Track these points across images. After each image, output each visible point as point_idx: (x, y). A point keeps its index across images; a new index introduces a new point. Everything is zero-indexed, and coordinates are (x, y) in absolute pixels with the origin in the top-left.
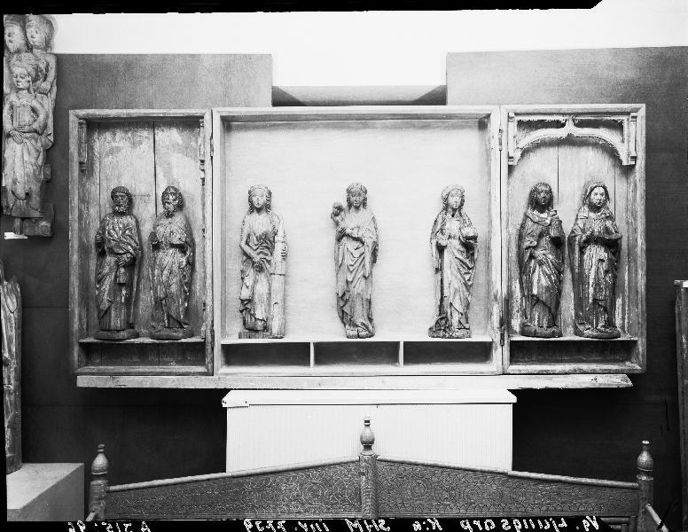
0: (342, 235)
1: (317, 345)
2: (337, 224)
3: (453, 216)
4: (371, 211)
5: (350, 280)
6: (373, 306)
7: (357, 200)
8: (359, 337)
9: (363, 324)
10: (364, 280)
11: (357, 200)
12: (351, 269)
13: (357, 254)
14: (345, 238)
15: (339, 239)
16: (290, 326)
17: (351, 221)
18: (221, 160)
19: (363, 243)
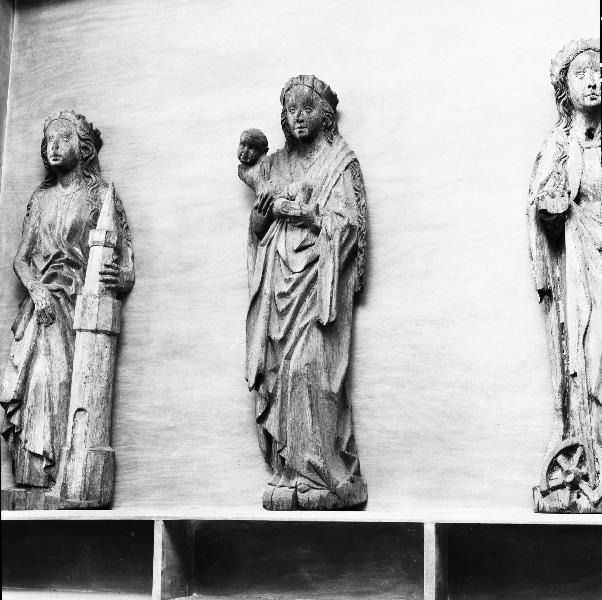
0: (266, 219)
1: (449, 534)
2: (252, 185)
3: (594, 186)
4: (346, 145)
5: (277, 336)
6: (129, 351)
7: (314, 120)
8: (296, 506)
9: (312, 467)
10: (317, 338)
11: (314, 120)
12: (282, 305)
13: (299, 262)
14: (274, 226)
15: (258, 232)
16: (125, 481)
17: (287, 184)
18: (569, 400)
19: (316, 231)
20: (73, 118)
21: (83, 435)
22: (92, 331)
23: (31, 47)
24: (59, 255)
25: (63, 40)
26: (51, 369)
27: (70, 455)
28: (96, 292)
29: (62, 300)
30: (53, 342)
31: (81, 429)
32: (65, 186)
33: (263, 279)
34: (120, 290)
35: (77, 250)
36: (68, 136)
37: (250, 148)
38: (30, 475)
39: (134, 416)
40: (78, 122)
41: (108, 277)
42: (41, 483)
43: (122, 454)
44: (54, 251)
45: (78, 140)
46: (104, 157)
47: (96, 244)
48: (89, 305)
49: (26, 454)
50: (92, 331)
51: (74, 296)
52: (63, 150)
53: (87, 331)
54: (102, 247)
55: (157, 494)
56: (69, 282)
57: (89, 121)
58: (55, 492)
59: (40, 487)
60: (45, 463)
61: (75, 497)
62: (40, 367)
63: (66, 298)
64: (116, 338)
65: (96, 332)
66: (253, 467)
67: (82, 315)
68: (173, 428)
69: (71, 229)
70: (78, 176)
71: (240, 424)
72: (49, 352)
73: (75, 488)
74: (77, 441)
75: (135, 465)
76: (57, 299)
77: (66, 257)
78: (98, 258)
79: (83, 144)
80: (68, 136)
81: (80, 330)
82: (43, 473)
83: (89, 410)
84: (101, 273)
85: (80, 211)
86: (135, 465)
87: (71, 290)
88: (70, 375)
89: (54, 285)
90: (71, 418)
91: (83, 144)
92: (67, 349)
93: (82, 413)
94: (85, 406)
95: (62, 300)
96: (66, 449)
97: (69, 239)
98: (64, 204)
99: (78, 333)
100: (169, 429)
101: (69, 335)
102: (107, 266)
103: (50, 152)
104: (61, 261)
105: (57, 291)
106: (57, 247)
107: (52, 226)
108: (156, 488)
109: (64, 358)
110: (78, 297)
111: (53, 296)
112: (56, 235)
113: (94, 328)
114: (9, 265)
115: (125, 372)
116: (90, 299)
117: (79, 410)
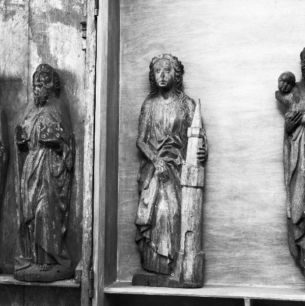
6: (211, 196)
16: (211, 268)
20: (171, 59)
21: (188, 243)
22: (194, 187)
23: (133, 11)
24: (168, 140)
25: (153, 8)
26: (168, 206)
27: (184, 258)
28: (195, 163)
29: (173, 167)
30: (168, 192)
31: (189, 243)
32: (166, 98)
33: (298, 161)
34: (203, 160)
35: (177, 137)
36: (169, 69)
37: (288, 83)
38: (160, 267)
39: (211, 232)
40: (174, 61)
41: (201, 156)
42: (166, 272)
43: (208, 254)
44: (164, 138)
45: (174, 71)
46: (187, 79)
47: (192, 136)
48: (192, 172)
49: (155, 255)
50: (194, 187)
51: (181, 166)
52: (168, 77)
53: (191, 187)
54: (197, 138)
55: (229, 276)
56: (176, 157)
57: (179, 60)
58: (175, 277)
59: (166, 274)
60: (168, 261)
61: (189, 280)
62: (162, 206)
63: (175, 166)
64: (203, 188)
65: (197, 187)
66: (286, 264)
67: (188, 178)
68: (237, 240)
69: (174, 125)
70: (173, 93)
71: (277, 239)
72: (167, 198)
73: (189, 274)
74: (188, 249)
75: (215, 260)
76: (170, 167)
77: (173, 142)
78: (193, 145)
79: (177, 74)
80: (169, 69)
81: (187, 186)
82: (167, 267)
83: (195, 232)
84: (198, 154)
85: (177, 114)
86: (215, 260)
87: (177, 161)
88: (179, 210)
89: (166, 158)
90: (183, 239)
91: (177, 74)
92: (177, 197)
93: (190, 233)
94: (192, 230)
95: (173, 167)
96: (181, 253)
97: (173, 130)
98: (166, 111)
99: (184, 189)
100: (234, 240)
101: (178, 188)
102: (200, 149)
103: (158, 76)
104: (169, 144)
105: (169, 162)
106: (166, 135)
107: (161, 122)
108: (228, 273)
109: (175, 200)
110: (184, 167)
111: (167, 165)
112: (164, 128)
113: (195, 185)
114: (134, 144)
115: (208, 207)
116: (192, 169)
117: (188, 232)
